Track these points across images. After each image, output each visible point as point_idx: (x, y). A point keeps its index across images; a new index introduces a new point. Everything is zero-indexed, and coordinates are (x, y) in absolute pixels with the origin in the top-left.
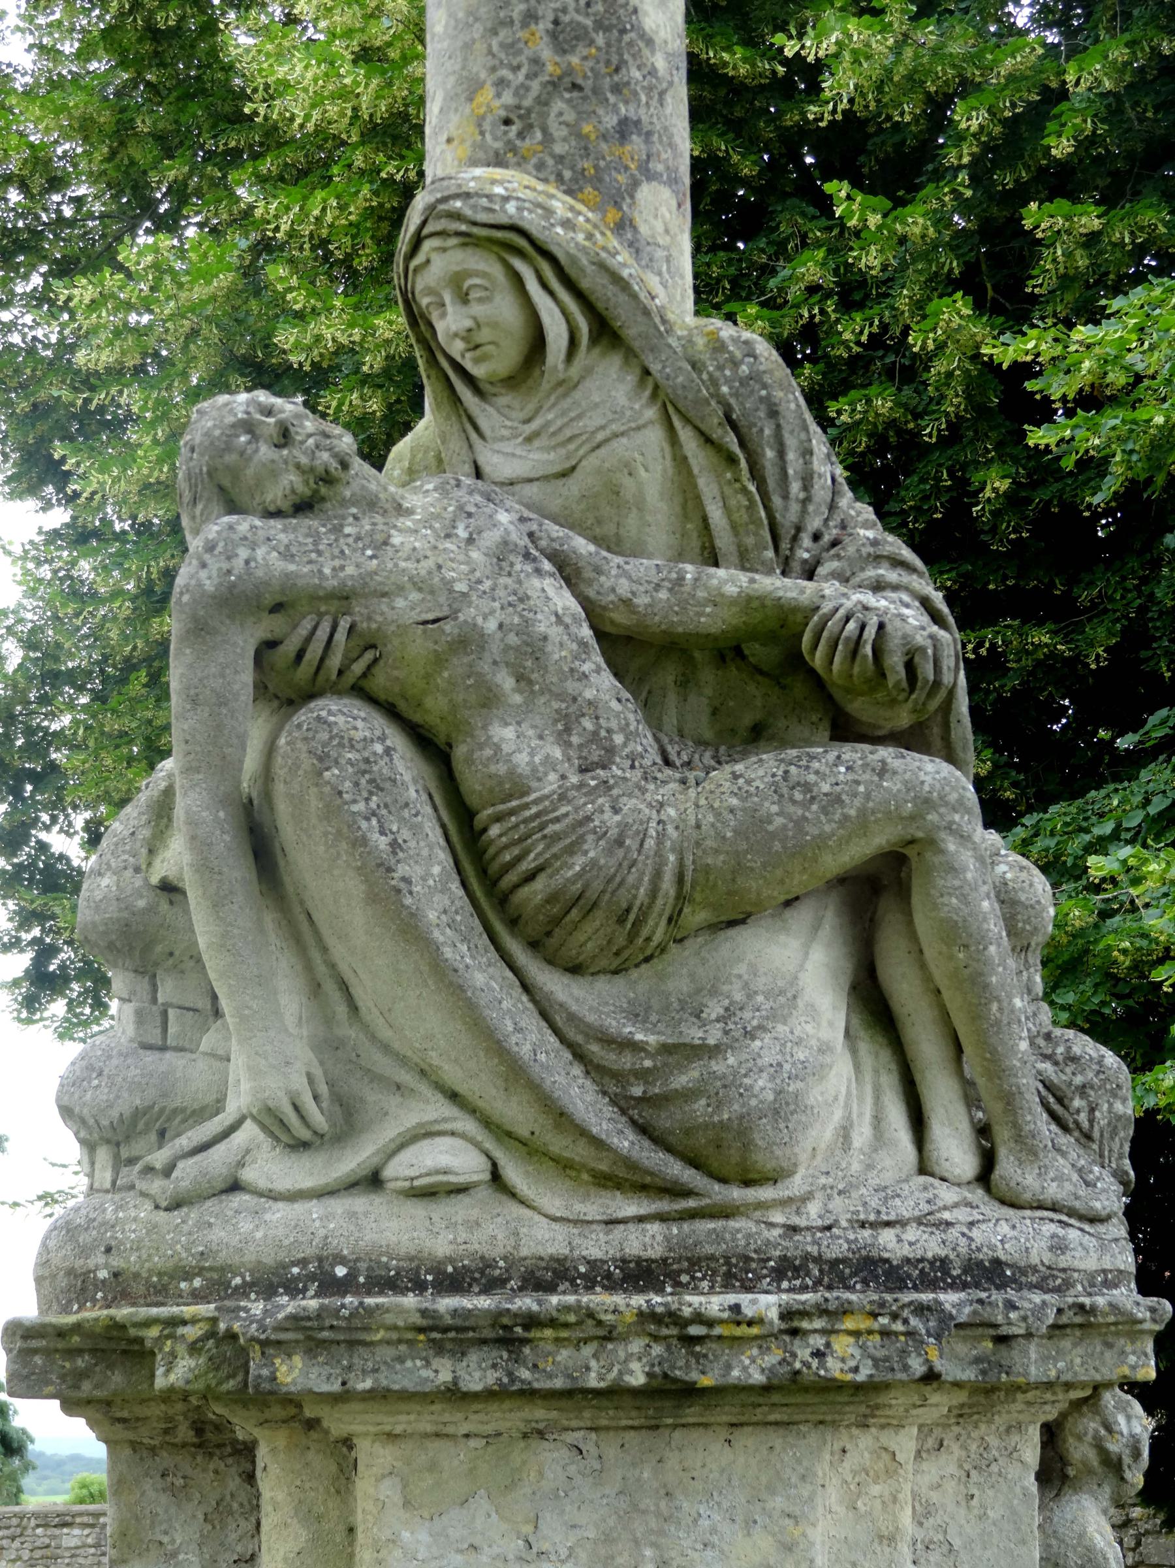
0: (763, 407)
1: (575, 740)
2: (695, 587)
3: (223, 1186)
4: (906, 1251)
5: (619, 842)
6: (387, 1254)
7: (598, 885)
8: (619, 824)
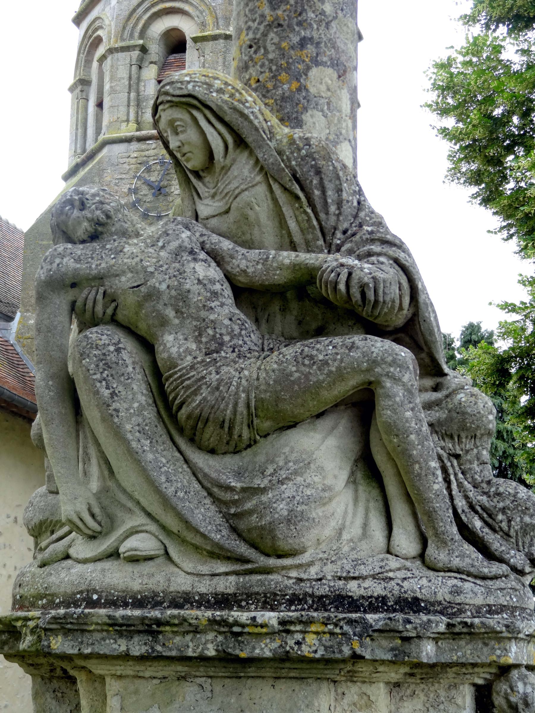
0: (313, 170)
1: (204, 340)
2: (272, 262)
3: (62, 556)
4: (362, 592)
5: (217, 388)
6: (114, 589)
7: (207, 410)
8: (217, 380)
